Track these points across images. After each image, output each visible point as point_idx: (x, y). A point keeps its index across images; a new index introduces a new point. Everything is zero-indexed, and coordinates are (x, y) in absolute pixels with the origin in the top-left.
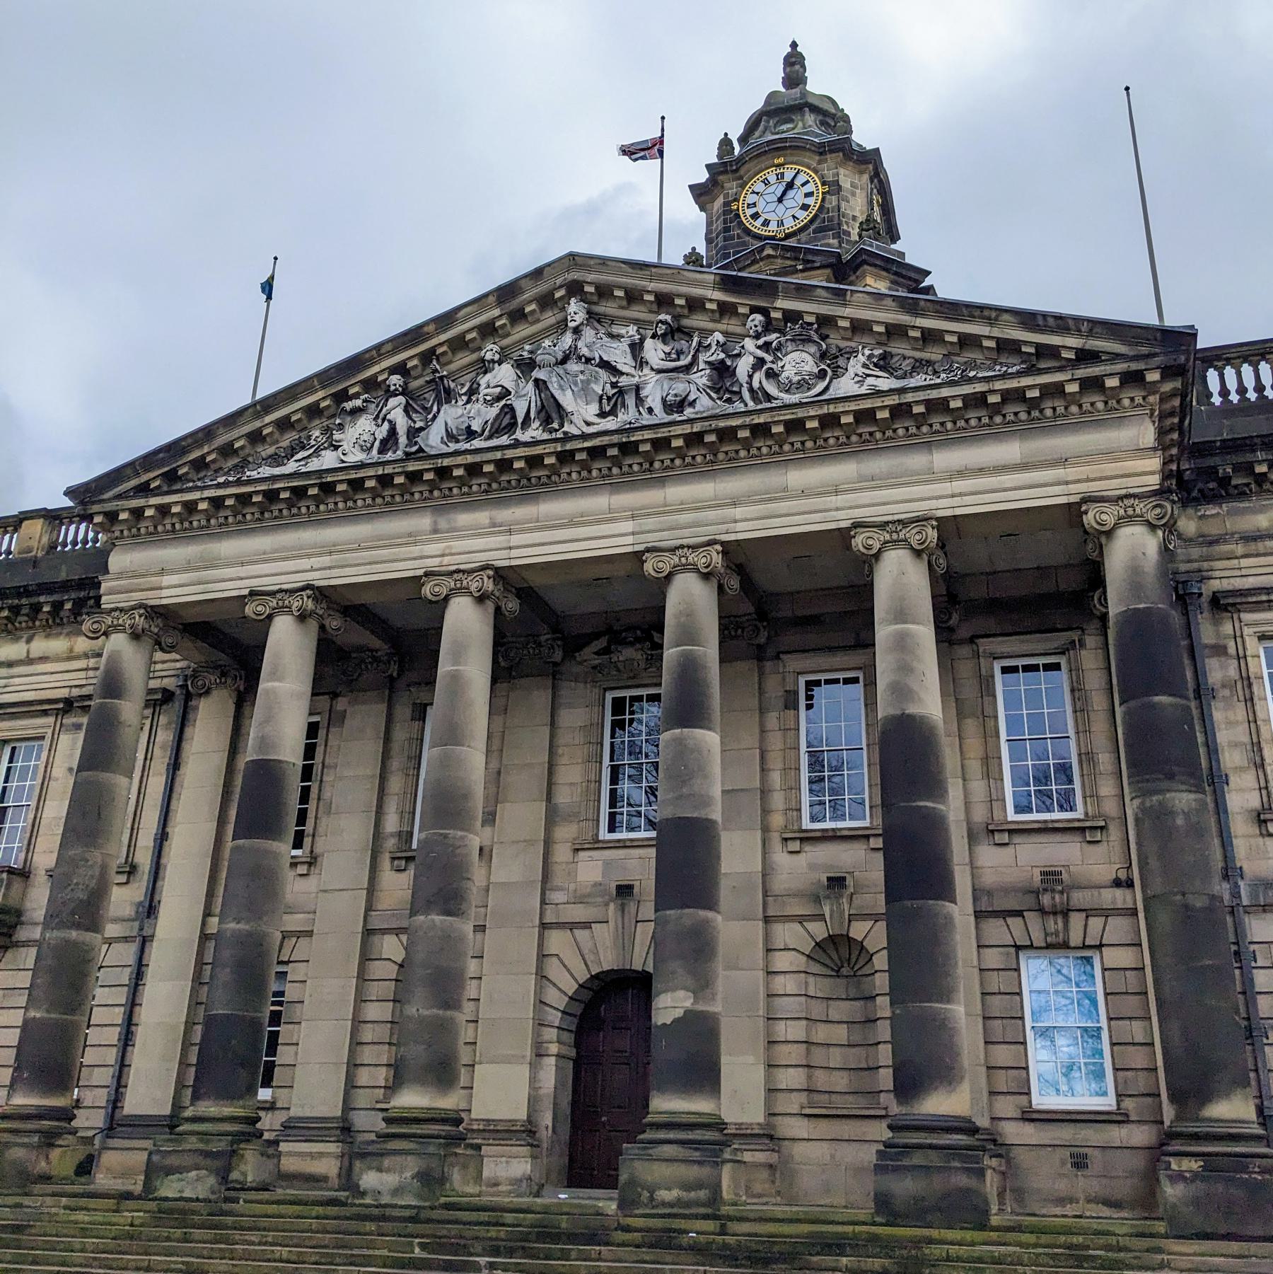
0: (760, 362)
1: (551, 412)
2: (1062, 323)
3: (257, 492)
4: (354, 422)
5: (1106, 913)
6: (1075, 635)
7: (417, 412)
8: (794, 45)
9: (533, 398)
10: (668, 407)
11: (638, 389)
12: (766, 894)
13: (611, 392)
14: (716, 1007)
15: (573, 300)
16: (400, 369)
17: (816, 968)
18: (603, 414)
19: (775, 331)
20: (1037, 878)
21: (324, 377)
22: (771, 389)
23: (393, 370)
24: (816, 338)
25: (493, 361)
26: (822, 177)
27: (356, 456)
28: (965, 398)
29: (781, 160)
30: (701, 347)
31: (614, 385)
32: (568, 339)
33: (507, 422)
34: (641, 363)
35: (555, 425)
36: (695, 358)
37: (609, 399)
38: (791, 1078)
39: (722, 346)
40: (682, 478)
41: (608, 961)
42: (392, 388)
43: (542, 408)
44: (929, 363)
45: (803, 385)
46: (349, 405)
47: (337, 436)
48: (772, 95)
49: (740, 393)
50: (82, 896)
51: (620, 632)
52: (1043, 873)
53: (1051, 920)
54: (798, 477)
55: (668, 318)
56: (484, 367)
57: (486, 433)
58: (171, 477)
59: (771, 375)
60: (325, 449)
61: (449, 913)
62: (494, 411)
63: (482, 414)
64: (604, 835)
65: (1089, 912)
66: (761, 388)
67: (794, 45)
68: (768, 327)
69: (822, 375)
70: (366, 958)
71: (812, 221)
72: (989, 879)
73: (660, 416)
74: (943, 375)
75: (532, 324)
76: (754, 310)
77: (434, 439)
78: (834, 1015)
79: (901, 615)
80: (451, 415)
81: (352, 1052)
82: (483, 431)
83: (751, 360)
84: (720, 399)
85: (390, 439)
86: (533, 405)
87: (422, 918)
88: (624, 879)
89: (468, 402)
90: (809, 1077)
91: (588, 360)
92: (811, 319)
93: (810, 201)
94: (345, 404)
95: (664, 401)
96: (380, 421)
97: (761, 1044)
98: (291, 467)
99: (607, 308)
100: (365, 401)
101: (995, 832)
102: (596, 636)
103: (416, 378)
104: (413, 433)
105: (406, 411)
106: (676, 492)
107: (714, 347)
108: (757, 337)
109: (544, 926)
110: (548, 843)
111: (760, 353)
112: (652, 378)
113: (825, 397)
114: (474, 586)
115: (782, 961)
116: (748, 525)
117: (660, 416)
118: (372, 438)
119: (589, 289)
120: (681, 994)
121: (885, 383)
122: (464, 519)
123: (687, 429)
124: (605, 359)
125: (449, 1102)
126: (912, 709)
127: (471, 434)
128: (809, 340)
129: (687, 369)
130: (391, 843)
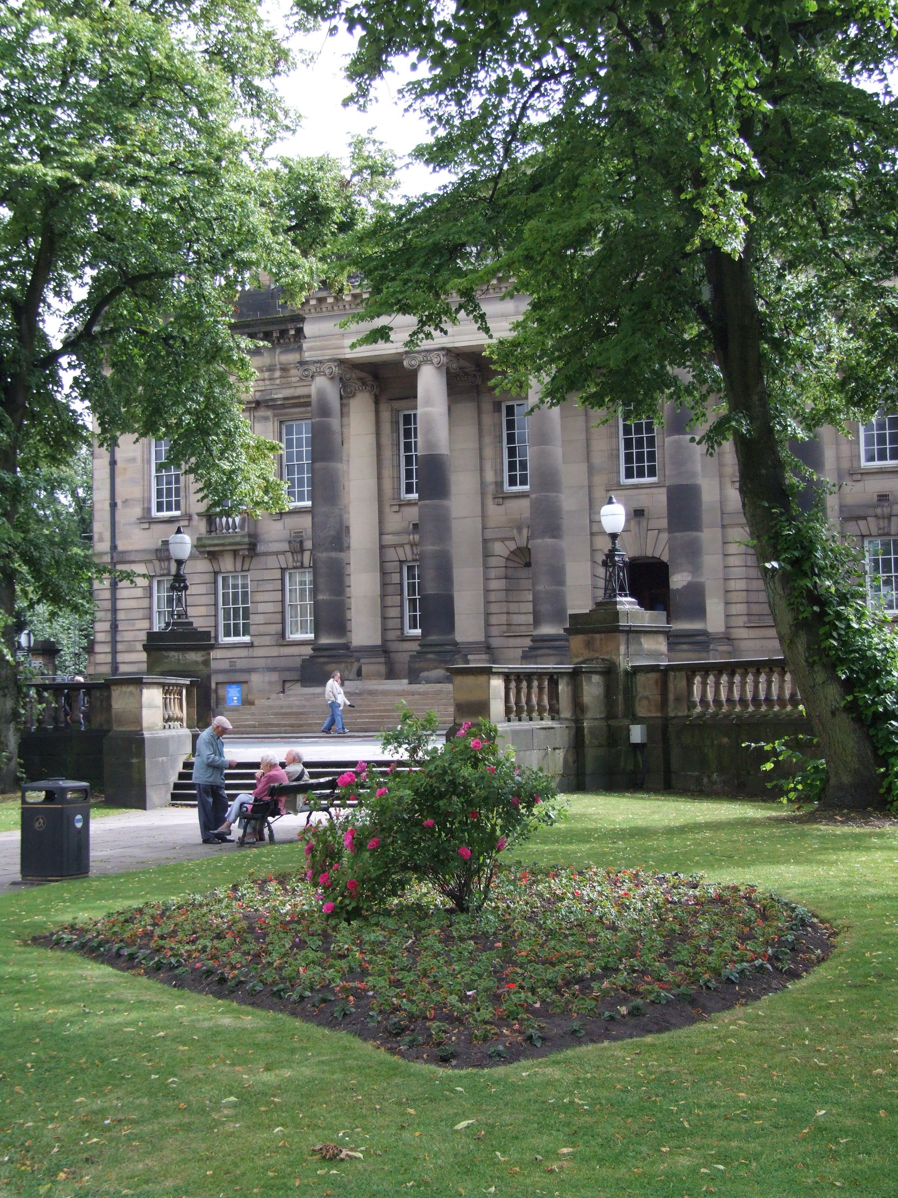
5: (204, 1020)
12: (722, 513)
14: (702, 580)
17: (752, 551)
20: (876, 498)
38: (740, 609)
50: (332, 533)
53: (881, 521)
61: (554, 537)
64: (624, 481)
70: (487, 555)
72: (849, 500)
81: (486, 608)
87: (540, 541)
88: (638, 505)
90: (749, 608)
97: (722, 592)
101: (858, 474)
109: (592, 534)
115: (733, 549)
120: (685, 574)
130: (491, 489)
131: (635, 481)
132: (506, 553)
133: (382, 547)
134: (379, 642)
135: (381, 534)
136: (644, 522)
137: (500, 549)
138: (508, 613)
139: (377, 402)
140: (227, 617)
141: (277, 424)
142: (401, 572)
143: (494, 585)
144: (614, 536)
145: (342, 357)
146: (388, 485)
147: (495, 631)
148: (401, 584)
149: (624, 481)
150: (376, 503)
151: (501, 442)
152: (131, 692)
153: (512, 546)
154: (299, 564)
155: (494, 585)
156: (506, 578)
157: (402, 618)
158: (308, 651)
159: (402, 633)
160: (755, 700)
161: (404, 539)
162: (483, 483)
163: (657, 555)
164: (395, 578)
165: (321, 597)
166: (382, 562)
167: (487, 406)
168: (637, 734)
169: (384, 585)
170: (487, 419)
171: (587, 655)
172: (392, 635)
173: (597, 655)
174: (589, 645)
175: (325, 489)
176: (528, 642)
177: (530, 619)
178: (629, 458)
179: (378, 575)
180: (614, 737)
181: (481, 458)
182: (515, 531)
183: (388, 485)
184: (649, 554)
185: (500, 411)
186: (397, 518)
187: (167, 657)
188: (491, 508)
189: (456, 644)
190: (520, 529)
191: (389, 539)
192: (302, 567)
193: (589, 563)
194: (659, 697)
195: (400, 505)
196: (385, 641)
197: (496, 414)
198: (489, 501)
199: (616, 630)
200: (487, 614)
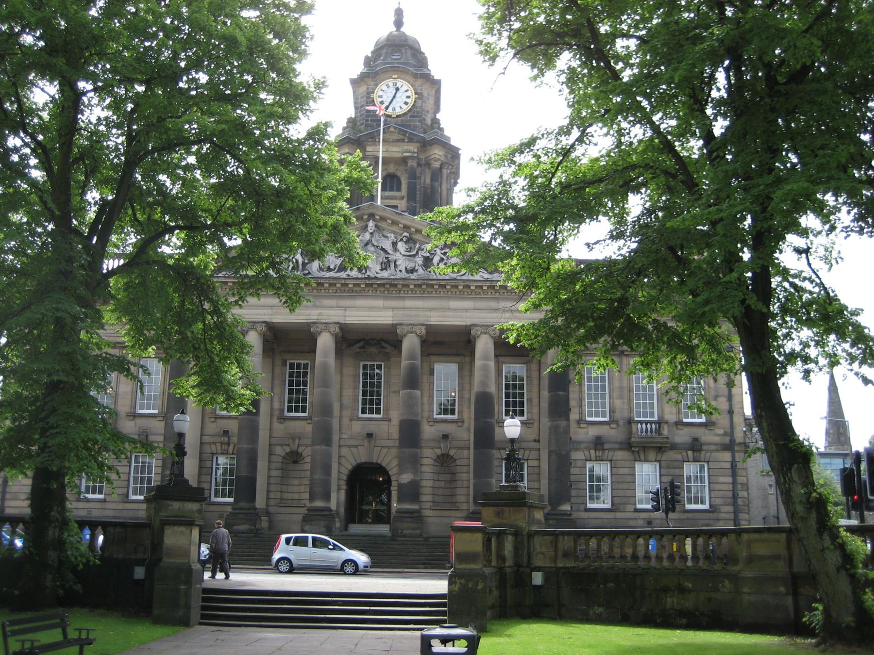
0: (442, 260)
5: (531, 450)
10: (407, 271)
17: (436, 464)
18: (382, 269)
26: (415, 90)
30: (420, 249)
31: (387, 258)
32: (367, 236)
34: (396, 250)
36: (417, 253)
40: (411, 298)
41: (364, 459)
48: (391, 33)
54: (453, 304)
55: (408, 235)
61: (328, 446)
64: (361, 415)
65: (707, 451)
71: (409, 111)
78: (440, 478)
83: (439, 258)
88: (369, 431)
93: (409, 100)
95: (406, 268)
99: (383, 225)
102: (359, 341)
106: (409, 303)
108: (442, 249)
114: (332, 330)
116: (436, 319)
117: (404, 275)
122: (327, 302)
125: (327, 505)
126: (488, 390)
127: (329, 269)
129: (414, 256)
130: (276, 413)
131: (367, 416)
132: (283, 454)
133: (201, 443)
135: (202, 435)
136: (373, 442)
137: (279, 450)
140: (135, 482)
143: (274, 473)
147: (272, 502)
149: (361, 415)
150: (200, 415)
152: (182, 532)
153: (288, 450)
155: (274, 473)
157: (128, 487)
158: (229, 509)
160: (635, 557)
161: (217, 439)
162: (272, 409)
163: (379, 462)
164: (208, 464)
166: (201, 453)
167: (278, 362)
168: (538, 578)
169: (200, 467)
171: (497, 520)
173: (505, 521)
174: (498, 514)
176: (304, 511)
177: (307, 496)
178: (364, 402)
180: (521, 579)
182: (291, 441)
184: (374, 461)
186: (213, 425)
187: (169, 505)
188: (276, 425)
189: (256, 509)
190: (293, 439)
191: (206, 439)
194: (553, 553)
195: (216, 418)
198: (275, 420)
199: (525, 505)
200: (268, 491)
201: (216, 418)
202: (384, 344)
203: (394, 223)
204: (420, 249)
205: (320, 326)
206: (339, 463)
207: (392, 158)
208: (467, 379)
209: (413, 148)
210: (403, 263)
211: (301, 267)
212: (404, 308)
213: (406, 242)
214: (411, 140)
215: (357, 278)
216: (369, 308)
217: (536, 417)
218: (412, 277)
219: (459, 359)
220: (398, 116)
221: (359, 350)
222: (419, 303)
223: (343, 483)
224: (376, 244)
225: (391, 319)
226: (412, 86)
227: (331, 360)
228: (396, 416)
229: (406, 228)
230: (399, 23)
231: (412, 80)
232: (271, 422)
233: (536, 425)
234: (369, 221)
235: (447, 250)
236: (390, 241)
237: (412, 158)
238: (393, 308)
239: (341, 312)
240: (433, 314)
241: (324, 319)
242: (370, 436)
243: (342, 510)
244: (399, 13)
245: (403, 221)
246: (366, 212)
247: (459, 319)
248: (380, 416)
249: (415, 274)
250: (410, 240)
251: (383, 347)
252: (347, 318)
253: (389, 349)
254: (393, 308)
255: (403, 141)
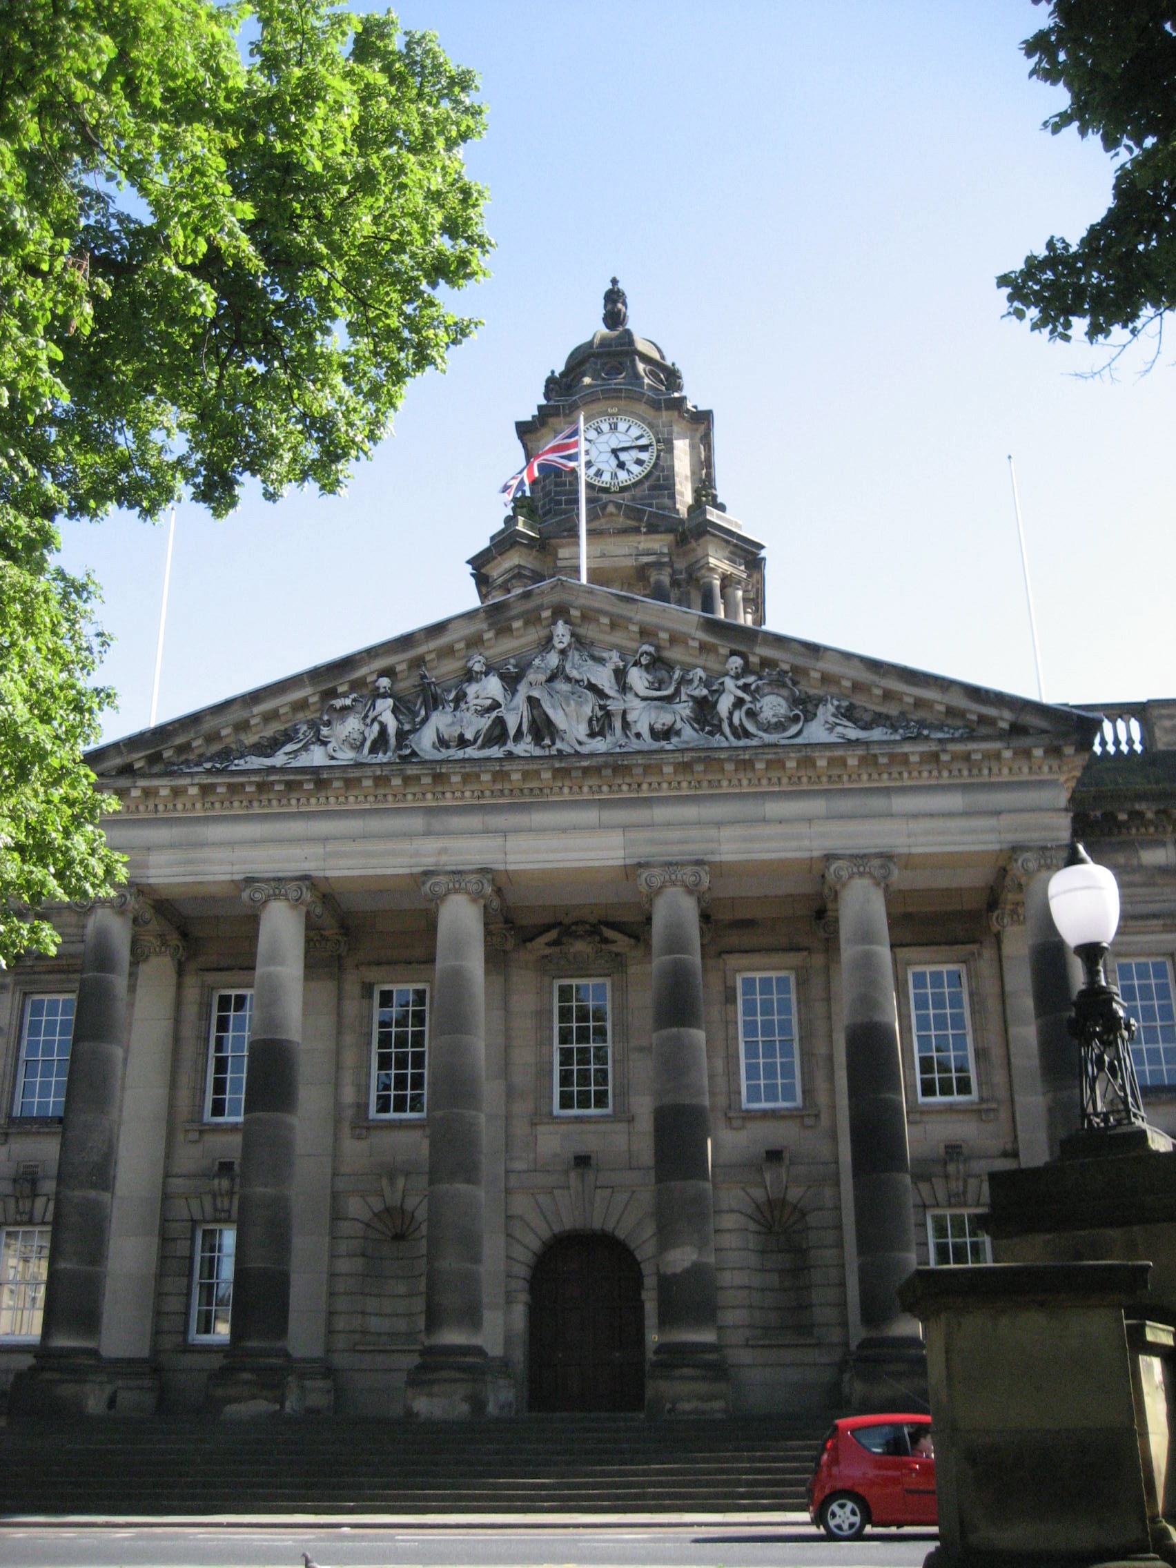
0: (739, 702)
1: (542, 728)
2: (1000, 699)
3: (250, 783)
4: (343, 720)
6: (973, 947)
7: (403, 714)
8: (614, 281)
9: (525, 714)
10: (655, 734)
11: (624, 713)
13: (600, 714)
15: (560, 623)
16: (388, 672)
17: (752, 1226)
18: (592, 735)
19: (752, 673)
20: (942, 1150)
21: (316, 675)
22: (751, 728)
23: (385, 673)
24: (789, 683)
25: (481, 672)
26: (656, 434)
27: (346, 756)
28: (922, 754)
29: (615, 410)
30: (683, 681)
31: (602, 707)
32: (553, 659)
33: (498, 733)
34: (624, 688)
35: (547, 741)
36: (677, 692)
37: (598, 720)
39: (707, 684)
42: (382, 690)
43: (533, 722)
44: (888, 717)
45: (780, 726)
46: (339, 703)
47: (325, 731)
49: (720, 726)
51: (569, 927)
52: (946, 1147)
55: (652, 649)
56: (470, 676)
57: (479, 741)
58: (154, 759)
59: (751, 714)
60: (313, 743)
61: (469, 1181)
62: (485, 723)
63: (475, 725)
66: (741, 725)
67: (614, 281)
68: (746, 669)
69: (796, 719)
70: (337, 1216)
71: (647, 476)
73: (648, 743)
74: (901, 731)
75: (517, 638)
76: (733, 653)
77: (425, 741)
79: (866, 936)
80: (440, 722)
82: (476, 740)
83: (732, 699)
84: (703, 730)
85: (380, 742)
86: (525, 720)
88: (581, 1149)
89: (455, 709)
91: (577, 681)
92: (786, 667)
94: (333, 702)
95: (652, 729)
96: (368, 721)
98: (279, 760)
100: (354, 700)
102: (548, 928)
103: (402, 680)
104: (402, 735)
105: (393, 712)
107: (696, 683)
108: (737, 677)
110: (508, 1117)
111: (740, 694)
112: (637, 703)
113: (798, 741)
117: (648, 743)
118: (361, 737)
119: (575, 613)
120: (688, 1249)
121: (853, 733)
123: (678, 757)
124: (593, 682)
127: (462, 742)
128: (784, 685)
129: (668, 699)
130: (349, 1113)
131: (575, 1112)
134: (145, 1353)
135: (167, 1175)
138: (363, 1313)
139: (180, 971)
141: (18, 996)
142: (192, 1239)
144: (1091, 952)
145: (144, 881)
146: (184, 1096)
147: (341, 1342)
148: (191, 1258)
150: (164, 1125)
151: (369, 1043)
154: (25, 1218)
155: (344, 1266)
156: (363, 1255)
157: (187, 1314)
159: (185, 1340)
162: (338, 1105)
164: (181, 1248)
165: (62, 1265)
166: (165, 1220)
167: (352, 988)
169: (163, 1258)
170: (352, 1008)
172: (168, 1342)
175: (88, 1082)
179: (156, 1240)
181: (338, 1067)
182: (385, 1182)
183: (184, 1096)
184: (597, 1225)
185: (371, 997)
189: (287, 1355)
190: (392, 1179)
192: (30, 1222)
193: (502, 1237)
195: (201, 1132)
196: (155, 1351)
197: (365, 1002)
200: (331, 1314)
201: (201, 1132)
202: (609, 933)
203: (616, 624)
204: (683, 681)
205: (442, 879)
206: (509, 1235)
207: (616, 570)
208: (819, 1008)
209: (659, 543)
210: (643, 717)
211: (393, 741)
212: (651, 825)
213: (647, 668)
214: (653, 529)
215: (533, 758)
216: (564, 830)
217: (1002, 1093)
218: (669, 747)
219: (795, 959)
220: (623, 489)
221: (548, 951)
222: (690, 812)
223: (520, 1285)
224: (574, 674)
225: (621, 853)
226: (651, 426)
227: (475, 964)
228: (643, 1106)
229: (646, 633)
230: (614, 317)
231: (649, 413)
232: (336, 1138)
233: (1004, 1114)
234: (554, 623)
235: (751, 679)
236: (611, 666)
237: (658, 565)
238: (625, 827)
239: (495, 842)
240: (726, 832)
241: (451, 861)
242: (582, 1161)
243: (519, 1355)
244: (614, 297)
245: (638, 617)
246: (546, 600)
247: (794, 844)
248: (608, 1111)
249: (674, 740)
250: (657, 664)
251: (605, 941)
252: (510, 858)
253: (621, 942)
254: (625, 827)
255: (637, 530)
